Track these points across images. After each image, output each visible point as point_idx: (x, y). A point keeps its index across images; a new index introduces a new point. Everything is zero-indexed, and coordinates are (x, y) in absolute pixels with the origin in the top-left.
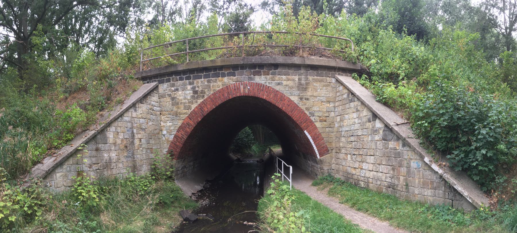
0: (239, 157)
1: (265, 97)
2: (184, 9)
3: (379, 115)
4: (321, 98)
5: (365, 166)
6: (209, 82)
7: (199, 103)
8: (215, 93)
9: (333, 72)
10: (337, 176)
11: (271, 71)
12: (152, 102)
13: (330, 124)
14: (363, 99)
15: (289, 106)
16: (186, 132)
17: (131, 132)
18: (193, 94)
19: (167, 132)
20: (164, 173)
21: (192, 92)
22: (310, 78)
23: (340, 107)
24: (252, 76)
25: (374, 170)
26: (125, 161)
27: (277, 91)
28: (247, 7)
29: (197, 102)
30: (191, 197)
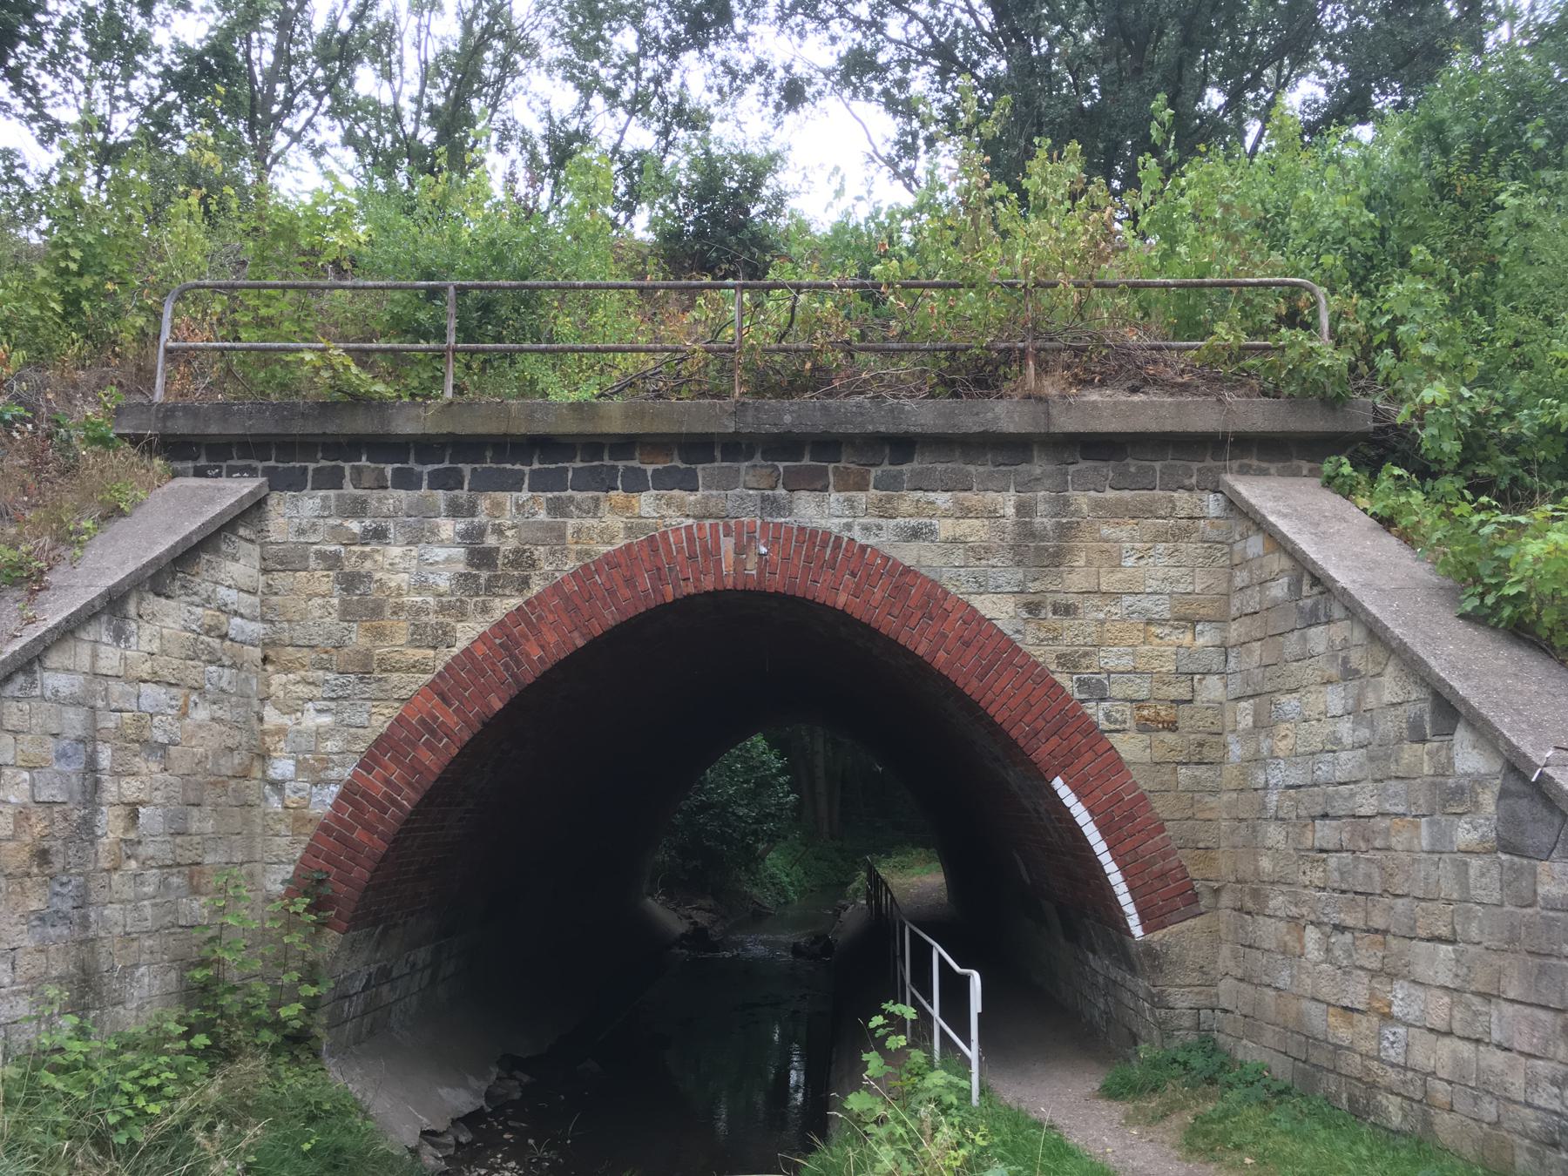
0: (702, 919)
1: (842, 600)
2: (408, 40)
3: (1463, 701)
4: (1147, 603)
5: (1401, 999)
6: (556, 508)
7: (498, 615)
8: (585, 567)
9: (1209, 463)
10: (1250, 1053)
11: (874, 473)
12: (222, 592)
13: (1201, 745)
14: (1373, 610)
15: (967, 644)
16: (415, 768)
17: (78, 765)
18: (470, 564)
19: (301, 766)
20: (263, 1012)
21: (460, 552)
22: (1082, 500)
23: (1250, 653)
24: (781, 492)
25: (1457, 1027)
26: (29, 942)
27: (907, 570)
28: (771, 75)
29: (485, 610)
30: (414, 1152)
